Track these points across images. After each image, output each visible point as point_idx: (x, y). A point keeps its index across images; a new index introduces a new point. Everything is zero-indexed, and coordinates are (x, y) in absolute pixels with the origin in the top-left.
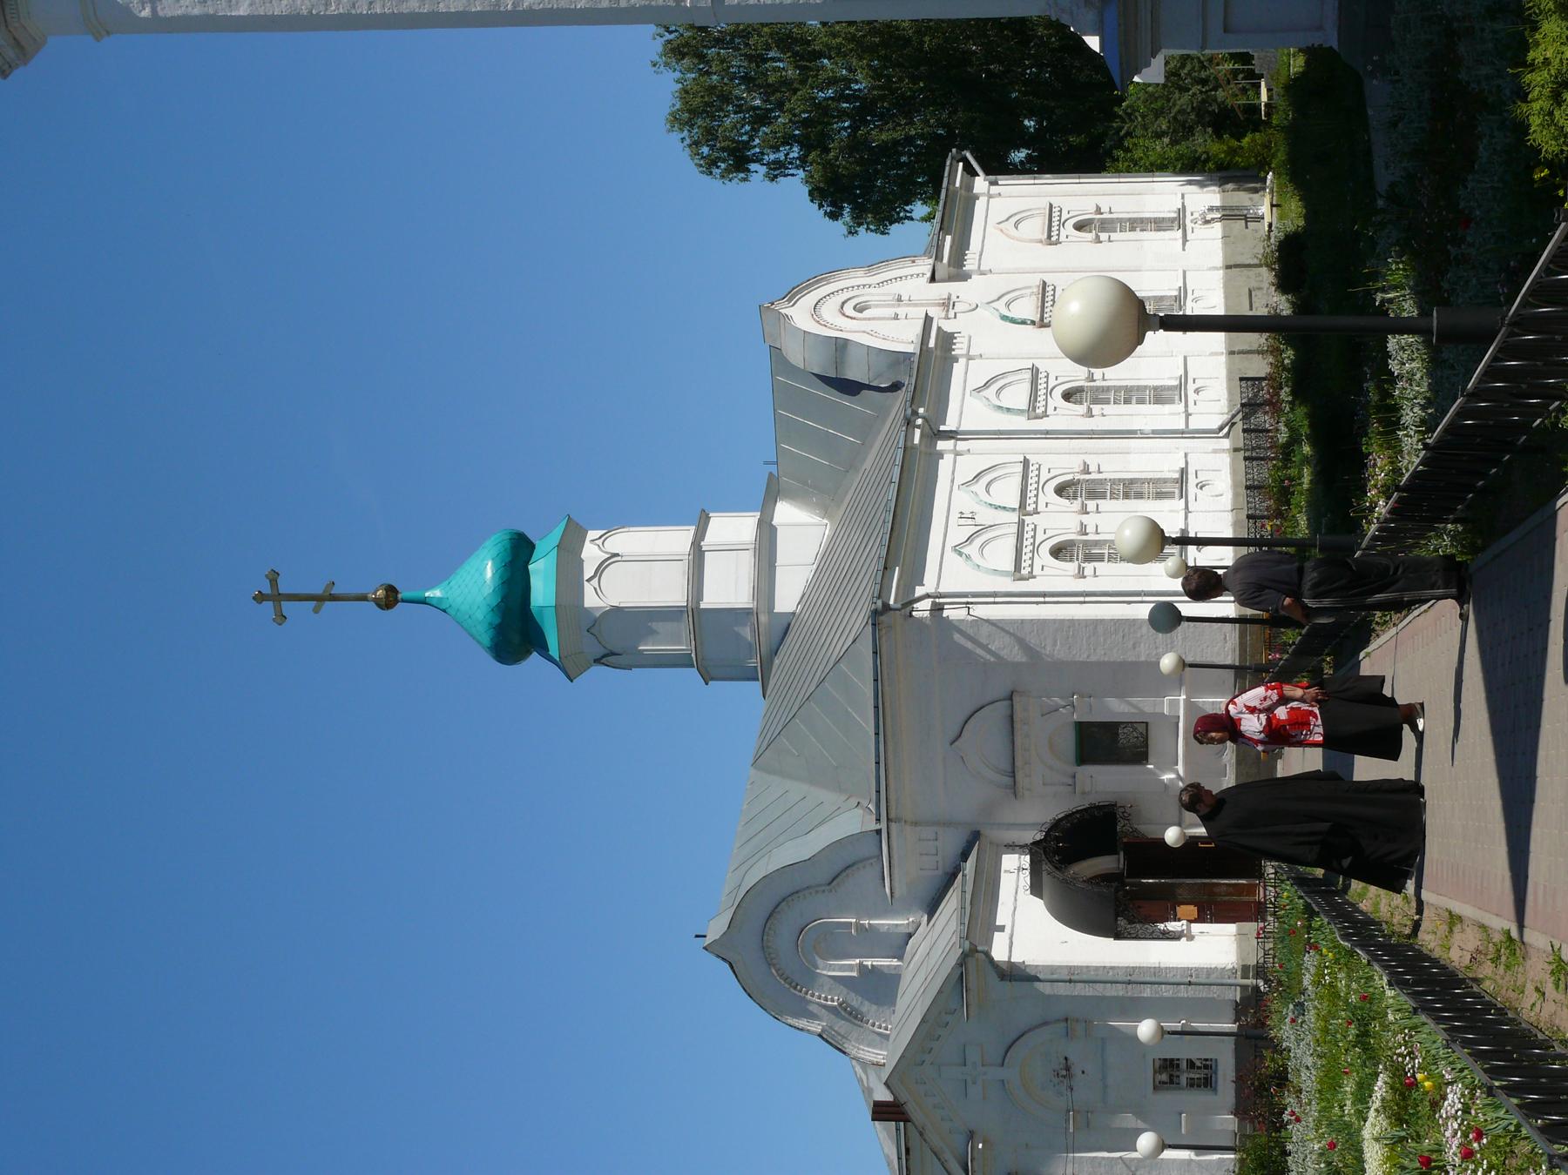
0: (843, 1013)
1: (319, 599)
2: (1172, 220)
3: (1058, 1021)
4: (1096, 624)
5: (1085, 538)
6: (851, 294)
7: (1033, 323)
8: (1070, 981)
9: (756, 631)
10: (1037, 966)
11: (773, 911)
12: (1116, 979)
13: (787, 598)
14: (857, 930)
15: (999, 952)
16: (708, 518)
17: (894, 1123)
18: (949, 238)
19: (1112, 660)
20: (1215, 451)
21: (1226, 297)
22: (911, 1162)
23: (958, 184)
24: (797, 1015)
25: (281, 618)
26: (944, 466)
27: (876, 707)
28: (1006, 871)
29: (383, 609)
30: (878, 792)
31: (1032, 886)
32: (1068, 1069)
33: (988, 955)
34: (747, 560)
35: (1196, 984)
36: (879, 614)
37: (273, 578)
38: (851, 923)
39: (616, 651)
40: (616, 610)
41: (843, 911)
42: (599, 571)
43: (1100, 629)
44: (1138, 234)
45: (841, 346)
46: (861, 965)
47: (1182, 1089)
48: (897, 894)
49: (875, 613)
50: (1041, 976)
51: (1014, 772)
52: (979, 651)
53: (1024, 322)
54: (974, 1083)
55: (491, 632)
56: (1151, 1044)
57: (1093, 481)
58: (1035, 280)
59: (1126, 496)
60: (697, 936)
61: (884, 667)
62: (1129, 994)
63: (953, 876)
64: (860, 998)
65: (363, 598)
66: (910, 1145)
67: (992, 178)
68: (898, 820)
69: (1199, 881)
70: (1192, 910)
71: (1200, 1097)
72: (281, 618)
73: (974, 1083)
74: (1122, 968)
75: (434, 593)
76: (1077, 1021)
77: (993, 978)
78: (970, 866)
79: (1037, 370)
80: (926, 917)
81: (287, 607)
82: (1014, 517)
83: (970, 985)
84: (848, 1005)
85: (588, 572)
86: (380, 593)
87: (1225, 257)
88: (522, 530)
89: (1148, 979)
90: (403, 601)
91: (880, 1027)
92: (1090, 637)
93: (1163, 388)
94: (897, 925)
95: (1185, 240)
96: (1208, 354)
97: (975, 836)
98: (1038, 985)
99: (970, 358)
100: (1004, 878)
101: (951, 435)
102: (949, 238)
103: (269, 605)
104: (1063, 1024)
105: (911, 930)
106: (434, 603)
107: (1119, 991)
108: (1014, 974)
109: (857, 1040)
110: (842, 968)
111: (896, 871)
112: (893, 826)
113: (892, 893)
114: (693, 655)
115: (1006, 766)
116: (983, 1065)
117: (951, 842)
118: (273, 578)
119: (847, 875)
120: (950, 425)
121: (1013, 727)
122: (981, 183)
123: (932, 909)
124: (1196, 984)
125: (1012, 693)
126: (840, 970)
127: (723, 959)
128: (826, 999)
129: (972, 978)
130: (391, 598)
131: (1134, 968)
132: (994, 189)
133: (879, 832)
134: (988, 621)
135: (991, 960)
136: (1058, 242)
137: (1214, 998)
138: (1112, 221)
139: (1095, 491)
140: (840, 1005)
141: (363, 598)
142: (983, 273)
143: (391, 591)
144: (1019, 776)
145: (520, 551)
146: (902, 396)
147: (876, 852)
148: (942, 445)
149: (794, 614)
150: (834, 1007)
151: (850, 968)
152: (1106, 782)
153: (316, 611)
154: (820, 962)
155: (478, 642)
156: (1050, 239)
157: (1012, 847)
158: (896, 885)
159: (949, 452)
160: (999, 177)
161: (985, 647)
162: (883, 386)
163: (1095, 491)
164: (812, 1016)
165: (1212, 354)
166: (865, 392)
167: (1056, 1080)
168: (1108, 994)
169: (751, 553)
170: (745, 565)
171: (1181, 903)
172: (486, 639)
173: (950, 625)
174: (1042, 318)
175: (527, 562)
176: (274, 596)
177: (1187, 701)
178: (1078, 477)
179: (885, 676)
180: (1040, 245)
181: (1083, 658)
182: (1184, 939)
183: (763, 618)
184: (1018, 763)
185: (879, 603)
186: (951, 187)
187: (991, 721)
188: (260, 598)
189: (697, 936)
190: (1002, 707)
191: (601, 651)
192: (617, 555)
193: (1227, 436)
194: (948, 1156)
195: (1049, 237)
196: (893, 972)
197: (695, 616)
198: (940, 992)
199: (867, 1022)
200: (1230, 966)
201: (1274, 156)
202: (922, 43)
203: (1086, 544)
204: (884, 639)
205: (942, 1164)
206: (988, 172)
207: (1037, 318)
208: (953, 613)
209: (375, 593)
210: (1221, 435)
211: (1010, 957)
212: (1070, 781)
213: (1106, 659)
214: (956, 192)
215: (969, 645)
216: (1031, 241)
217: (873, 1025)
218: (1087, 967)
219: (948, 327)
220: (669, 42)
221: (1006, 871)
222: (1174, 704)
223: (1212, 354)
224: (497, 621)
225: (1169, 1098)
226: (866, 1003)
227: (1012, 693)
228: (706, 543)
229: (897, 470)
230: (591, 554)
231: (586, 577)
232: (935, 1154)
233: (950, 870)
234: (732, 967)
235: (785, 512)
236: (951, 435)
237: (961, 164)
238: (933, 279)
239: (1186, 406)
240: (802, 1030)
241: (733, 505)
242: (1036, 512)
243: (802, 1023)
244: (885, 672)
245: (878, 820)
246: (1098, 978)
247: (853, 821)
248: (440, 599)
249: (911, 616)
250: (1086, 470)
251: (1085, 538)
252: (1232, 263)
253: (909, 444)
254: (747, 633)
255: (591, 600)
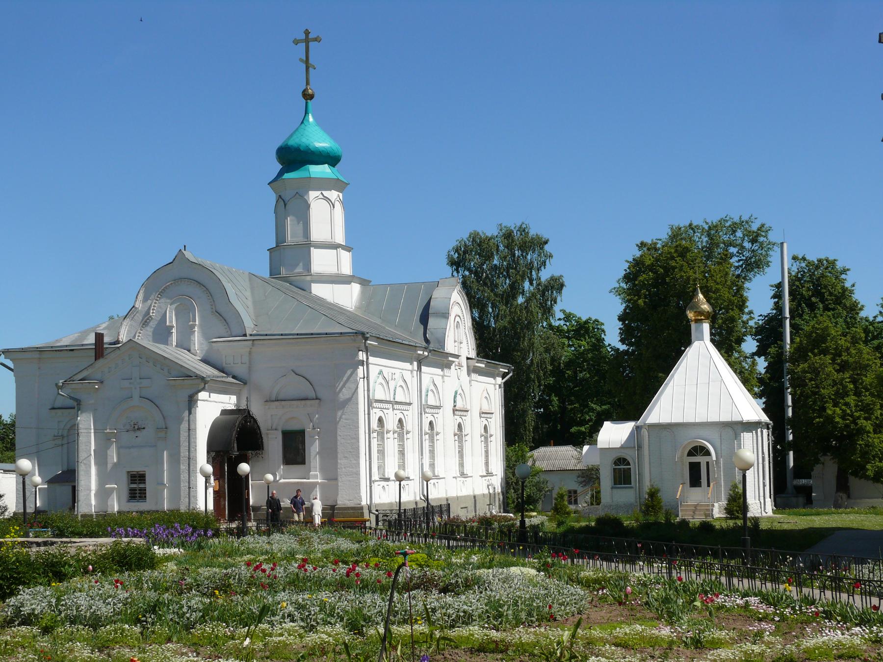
0: (146, 318)
2: (384, 475)
3: (166, 424)
4: (357, 439)
5: (405, 433)
7: (455, 406)
8: (189, 430)
9: (300, 275)
12: (191, 452)
13: (319, 290)
16: (349, 251)
18: (483, 366)
19: (338, 447)
20: (415, 493)
21: (465, 496)
22: (66, 352)
23: (501, 370)
24: (145, 292)
25: (296, 42)
26: (407, 365)
27: (312, 334)
28: (230, 397)
29: (303, 92)
30: (266, 335)
31: (225, 410)
32: (139, 429)
33: (203, 389)
35: (189, 491)
36: (364, 336)
37: (317, 39)
38: (195, 322)
39: (287, 206)
40: (308, 206)
41: (202, 318)
42: (326, 199)
43: (353, 441)
45: (445, 315)
46: (172, 327)
47: (128, 485)
48: (214, 344)
49: (363, 334)
51: (278, 401)
52: (342, 383)
53: (455, 402)
54: (130, 383)
55: (296, 145)
56: (238, 470)
57: (403, 436)
58: (469, 408)
60: (185, 246)
63: (223, 372)
64: (154, 326)
67: (503, 386)
68: (253, 345)
69: (226, 491)
71: (125, 494)
72: (296, 42)
73: (130, 383)
75: (311, 119)
76: (166, 433)
77: (190, 392)
80: (200, 359)
81: (302, 46)
82: (392, 400)
83: (186, 381)
85: (326, 193)
87: (478, 495)
89: (191, 467)
92: (350, 436)
93: (384, 469)
94: (195, 344)
95: (482, 476)
97: (245, 383)
98: (187, 413)
99: (443, 376)
100: (227, 396)
101: (419, 369)
102: (483, 366)
104: (164, 427)
105: (192, 351)
106: (306, 117)
107: (184, 452)
108: (191, 402)
110: (171, 317)
112: (251, 342)
114: (285, 244)
115: (280, 397)
117: (240, 370)
118: (317, 39)
119: (221, 320)
120: (424, 368)
121: (302, 400)
122: (499, 380)
123: (205, 361)
124: (189, 491)
125: (319, 399)
126: (170, 317)
127: (174, 259)
128: (153, 310)
129: (188, 382)
130: (308, 96)
131: (196, 460)
133: (245, 335)
134: (357, 387)
135: (200, 391)
136: (481, 417)
140: (150, 317)
141: (308, 83)
142: (470, 382)
143: (311, 97)
144: (276, 403)
145: (332, 160)
146: (424, 344)
147: (234, 334)
148: (415, 363)
149: (311, 293)
150: (149, 314)
151: (171, 321)
152: (274, 445)
153: (301, 60)
154: (174, 306)
155: (291, 136)
157: (238, 399)
159: (413, 368)
160: (503, 389)
161: (344, 386)
164: (145, 299)
165: (446, 491)
166: (422, 327)
167: (132, 423)
168: (181, 448)
169: (337, 272)
170: (332, 270)
171: (219, 482)
172: (293, 142)
174: (457, 410)
175: (328, 164)
176: (307, 39)
177: (317, 483)
179: (328, 338)
181: (339, 433)
183: (308, 278)
185: (368, 336)
186: (500, 366)
187: (305, 390)
188: (307, 33)
189: (185, 246)
190: (312, 394)
192: (334, 207)
193: (421, 499)
194: (90, 371)
195: (483, 413)
196: (169, 342)
197: (306, 246)
198: (182, 366)
199: (141, 330)
200: (198, 507)
201: (561, 516)
202: (517, 351)
203: (383, 433)
204: (348, 338)
206: (505, 383)
207: (457, 408)
208: (361, 371)
209: (310, 89)
210: (421, 495)
211: (200, 400)
212: (274, 427)
214: (497, 369)
215: (345, 379)
216: (481, 405)
217: (140, 333)
220: (513, 232)
221: (230, 397)
222: (316, 477)
223: (446, 491)
224: (302, 149)
225: (124, 479)
226: (152, 329)
227: (319, 399)
229: (407, 343)
230: (333, 195)
231: (323, 192)
235: (356, 288)
236: (419, 369)
237: (507, 371)
238: (468, 358)
239: (377, 481)
240: (137, 298)
242: (393, 409)
243: (141, 297)
245: (251, 335)
248: (308, 121)
249: (359, 351)
253: (418, 348)
254: (299, 269)
255: (313, 194)
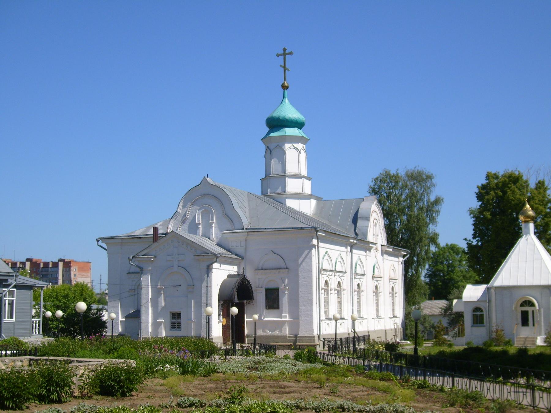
1: (284, 67)
3: (193, 283)
4: (311, 293)
5: (342, 291)
6: (378, 220)
7: (373, 274)
8: (207, 287)
10: (211, 277)
11: (216, 197)
13: (291, 203)
14: (211, 222)
15: (215, 265)
16: (310, 180)
17: (152, 233)
20: (348, 328)
22: (137, 239)
25: (278, 55)
26: (343, 249)
30: (256, 229)
33: (216, 262)
34: (299, 191)
37: (291, 53)
39: (272, 153)
40: (285, 153)
42: (296, 148)
43: (309, 295)
44: (375, 304)
45: (367, 219)
48: (224, 234)
49: (315, 228)
50: (208, 278)
57: (341, 292)
58: (382, 276)
59: (325, 301)
60: (207, 175)
61: (298, 231)
62: (203, 304)
65: (285, 80)
66: (142, 239)
67: (403, 263)
68: (248, 235)
70: (225, 323)
72: (278, 55)
74: (211, 302)
75: (286, 100)
76: (193, 289)
77: (208, 263)
78: (234, 256)
79: (364, 276)
81: (282, 57)
83: (205, 257)
84: (186, 220)
85: (295, 145)
86: (286, 84)
88: (305, 126)
90: (284, 91)
91: (179, 230)
94: (213, 235)
95: (390, 318)
96: (368, 325)
97: (243, 258)
99: (366, 256)
102: (391, 250)
103: (282, 52)
105: (211, 239)
106: (284, 100)
108: (209, 270)
109: (175, 223)
110: (199, 218)
111: (232, 234)
112: (246, 233)
113: (224, 233)
116: (178, 260)
117: (240, 251)
118: (291, 53)
120: (354, 251)
122: (401, 259)
123: (219, 245)
128: (188, 213)
130: (285, 87)
132: (400, 263)
133: (243, 229)
135: (214, 263)
136: (389, 281)
137: (201, 329)
138: (328, 293)
139: (339, 293)
140: (187, 218)
142: (383, 260)
143: (287, 88)
145: (299, 125)
148: (349, 248)
149: (286, 205)
150: (186, 216)
151: (199, 221)
152: (260, 297)
153: (281, 66)
154: (201, 211)
156: (390, 279)
158: (227, 234)
159: (347, 250)
160: (403, 265)
162: (357, 231)
163: (339, 293)
166: (353, 226)
173: (311, 250)
174: (375, 277)
178: (342, 288)
180: (389, 276)
181: (300, 290)
182: (218, 321)
183: (284, 196)
184: (266, 271)
185: (318, 229)
186: (401, 251)
188: (284, 50)
189: (207, 175)
190: (283, 265)
191: (272, 148)
192: (300, 153)
194: (148, 250)
195: (391, 279)
196: (197, 233)
197: (283, 176)
198: (203, 247)
199: (181, 226)
205: (146, 248)
206: (405, 261)
207: (375, 275)
208: (314, 251)
211: (214, 268)
213: (300, 297)
216: (390, 274)
218: (211, 292)
219: (372, 250)
222: (286, 317)
224: (281, 118)
227: (288, 269)
228: (304, 179)
230: (300, 146)
231: (294, 144)
232: (149, 246)
233: (231, 250)
234: (198, 185)
235: (313, 202)
237: (406, 254)
238: (382, 245)
241: (313, 187)
242: (335, 276)
243: (181, 206)
244: (296, 231)
245: (247, 229)
246: (208, 295)
247: (246, 223)
250: (344, 290)
251: (342, 291)
252: (387, 332)
253: (350, 238)
255: (287, 146)
